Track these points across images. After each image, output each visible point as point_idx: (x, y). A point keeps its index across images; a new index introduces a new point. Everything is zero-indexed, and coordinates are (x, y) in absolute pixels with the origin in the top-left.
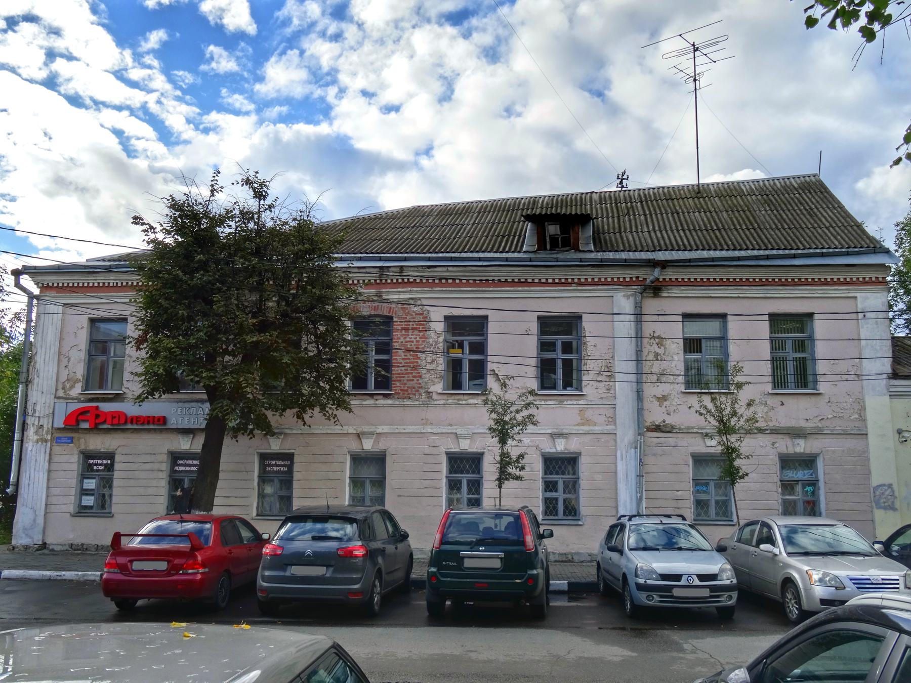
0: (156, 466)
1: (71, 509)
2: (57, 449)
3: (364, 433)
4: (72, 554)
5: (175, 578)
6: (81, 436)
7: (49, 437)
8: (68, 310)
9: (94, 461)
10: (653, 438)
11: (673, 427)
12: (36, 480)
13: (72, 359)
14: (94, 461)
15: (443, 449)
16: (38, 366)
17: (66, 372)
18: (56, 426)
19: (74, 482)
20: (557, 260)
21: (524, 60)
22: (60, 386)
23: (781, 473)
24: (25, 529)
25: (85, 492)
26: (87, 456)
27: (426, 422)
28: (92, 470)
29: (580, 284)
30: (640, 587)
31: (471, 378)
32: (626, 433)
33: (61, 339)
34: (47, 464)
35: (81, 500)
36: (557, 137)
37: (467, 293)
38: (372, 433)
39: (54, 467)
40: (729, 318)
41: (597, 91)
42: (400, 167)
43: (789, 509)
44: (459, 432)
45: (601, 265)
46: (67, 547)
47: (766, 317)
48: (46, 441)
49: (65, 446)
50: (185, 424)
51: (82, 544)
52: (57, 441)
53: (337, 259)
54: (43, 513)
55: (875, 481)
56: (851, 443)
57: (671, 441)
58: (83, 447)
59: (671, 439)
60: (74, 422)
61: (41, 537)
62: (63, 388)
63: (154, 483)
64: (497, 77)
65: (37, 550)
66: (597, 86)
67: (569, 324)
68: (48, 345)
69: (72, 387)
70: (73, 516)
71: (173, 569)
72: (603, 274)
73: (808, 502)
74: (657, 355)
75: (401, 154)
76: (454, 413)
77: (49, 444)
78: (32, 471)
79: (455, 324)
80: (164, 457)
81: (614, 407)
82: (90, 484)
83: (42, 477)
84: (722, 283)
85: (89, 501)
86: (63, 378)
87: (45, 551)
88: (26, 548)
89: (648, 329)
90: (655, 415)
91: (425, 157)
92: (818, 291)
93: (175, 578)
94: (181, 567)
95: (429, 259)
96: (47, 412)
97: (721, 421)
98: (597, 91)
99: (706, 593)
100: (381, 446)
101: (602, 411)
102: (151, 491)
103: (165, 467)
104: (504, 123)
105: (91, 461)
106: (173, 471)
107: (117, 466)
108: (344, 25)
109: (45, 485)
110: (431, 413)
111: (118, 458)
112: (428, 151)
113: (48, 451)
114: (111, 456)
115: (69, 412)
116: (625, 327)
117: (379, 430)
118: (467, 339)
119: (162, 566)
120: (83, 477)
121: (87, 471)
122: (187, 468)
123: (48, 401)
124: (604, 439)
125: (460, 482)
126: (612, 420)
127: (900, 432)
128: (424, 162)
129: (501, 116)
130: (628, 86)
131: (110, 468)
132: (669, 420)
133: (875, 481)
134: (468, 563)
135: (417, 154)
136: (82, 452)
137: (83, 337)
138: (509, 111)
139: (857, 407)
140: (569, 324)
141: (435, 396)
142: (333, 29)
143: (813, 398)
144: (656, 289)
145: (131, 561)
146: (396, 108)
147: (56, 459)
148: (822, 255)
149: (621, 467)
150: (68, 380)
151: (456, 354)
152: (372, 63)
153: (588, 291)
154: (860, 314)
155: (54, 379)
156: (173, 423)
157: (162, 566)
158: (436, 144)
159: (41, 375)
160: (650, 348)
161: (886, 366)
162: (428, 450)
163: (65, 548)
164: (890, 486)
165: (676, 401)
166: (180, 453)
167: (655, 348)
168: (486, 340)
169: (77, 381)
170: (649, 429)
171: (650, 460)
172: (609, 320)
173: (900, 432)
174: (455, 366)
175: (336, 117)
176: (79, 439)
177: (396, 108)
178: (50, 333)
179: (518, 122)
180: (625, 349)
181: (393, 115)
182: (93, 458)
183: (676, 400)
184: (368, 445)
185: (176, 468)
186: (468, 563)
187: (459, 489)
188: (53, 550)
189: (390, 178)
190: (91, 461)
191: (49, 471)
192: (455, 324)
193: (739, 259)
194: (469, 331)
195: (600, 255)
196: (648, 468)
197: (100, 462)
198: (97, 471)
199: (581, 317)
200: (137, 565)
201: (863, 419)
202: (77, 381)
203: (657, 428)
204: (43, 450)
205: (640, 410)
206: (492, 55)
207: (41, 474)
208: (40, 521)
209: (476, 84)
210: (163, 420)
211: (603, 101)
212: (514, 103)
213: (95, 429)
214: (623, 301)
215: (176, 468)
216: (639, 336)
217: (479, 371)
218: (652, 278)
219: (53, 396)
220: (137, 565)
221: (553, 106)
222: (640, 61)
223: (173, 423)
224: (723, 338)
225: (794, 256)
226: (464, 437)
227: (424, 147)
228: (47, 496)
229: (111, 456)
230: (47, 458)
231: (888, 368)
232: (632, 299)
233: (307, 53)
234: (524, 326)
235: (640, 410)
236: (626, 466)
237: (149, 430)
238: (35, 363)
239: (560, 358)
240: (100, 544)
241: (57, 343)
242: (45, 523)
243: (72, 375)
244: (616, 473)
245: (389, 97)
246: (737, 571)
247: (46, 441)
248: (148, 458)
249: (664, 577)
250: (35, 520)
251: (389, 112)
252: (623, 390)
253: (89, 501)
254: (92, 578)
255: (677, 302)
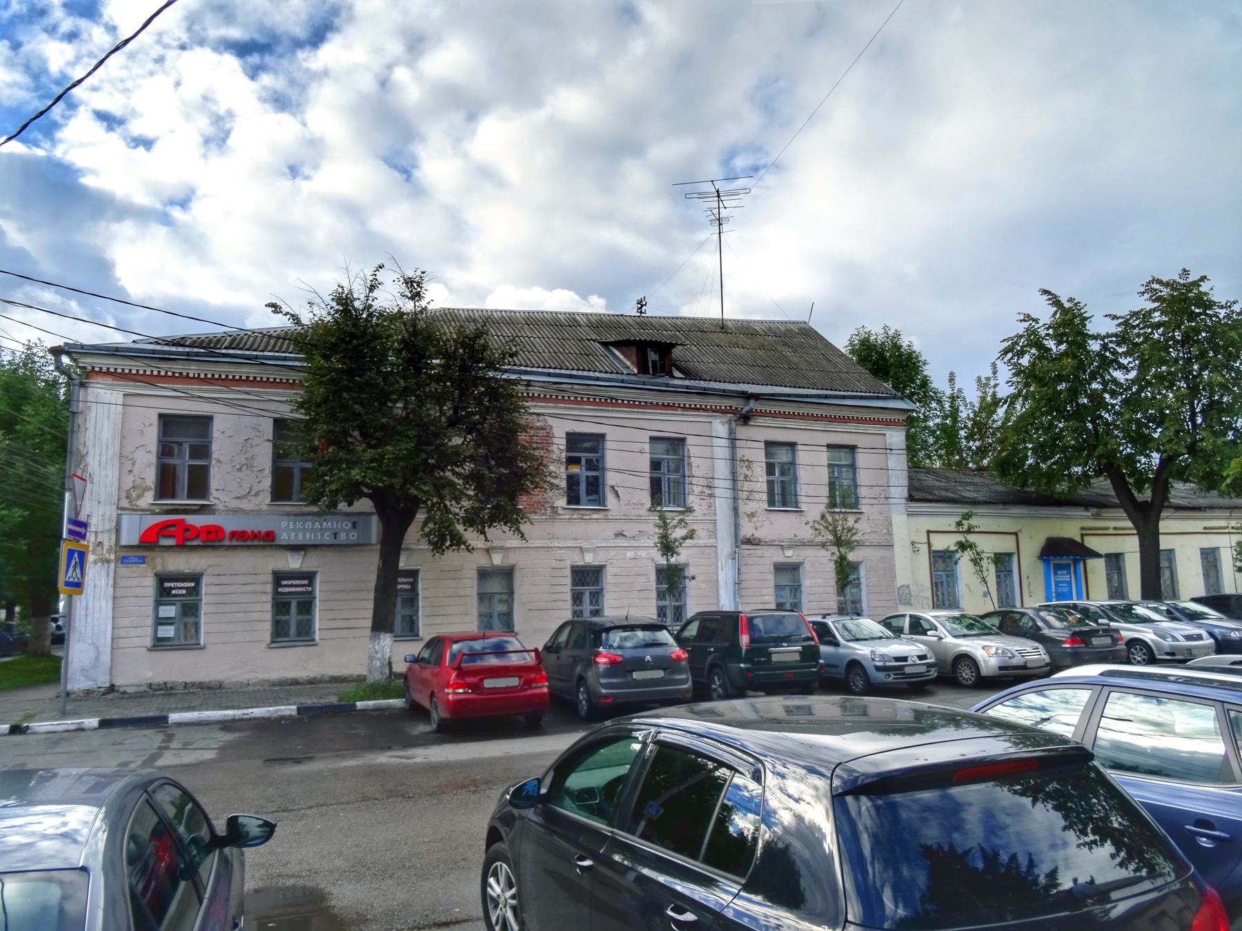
0: (259, 588)
1: (148, 642)
2: (123, 571)
3: (494, 548)
4: (153, 696)
5: (529, 692)
6: (157, 554)
7: (112, 557)
8: (130, 401)
9: (172, 585)
10: (746, 550)
11: (760, 540)
12: (97, 609)
13: (138, 462)
14: (172, 585)
15: (569, 563)
16: (90, 469)
17: (131, 478)
18: (124, 542)
19: (150, 610)
20: (667, 385)
21: (326, 115)
22: (124, 495)
23: (479, 586)
24: (83, 670)
25: (167, 621)
26: (162, 579)
27: (553, 537)
28: (169, 595)
29: (684, 408)
30: (878, 669)
31: (588, 493)
32: (725, 546)
33: (123, 438)
34: (111, 590)
35: (156, 631)
36: (350, 210)
37: (588, 411)
38: (502, 548)
39: (120, 593)
40: (800, 447)
41: (402, 166)
42: (142, 215)
43: (842, 611)
44: (584, 545)
45: (688, 392)
46: (144, 688)
47: (762, 445)
48: (108, 561)
49: (135, 568)
50: (300, 539)
51: (165, 683)
52: (123, 561)
53: (506, 371)
54: (108, 649)
55: (899, 583)
56: (881, 553)
57: (759, 553)
58: (159, 568)
59: (759, 551)
60: (150, 540)
61: (107, 678)
62: (127, 497)
63: (258, 607)
64: (284, 128)
65: (104, 694)
66: (403, 162)
67: (677, 443)
68: (104, 441)
69: (140, 496)
70: (150, 650)
71: (528, 683)
72: (703, 398)
73: (485, 615)
74: (746, 476)
75: (142, 199)
76: (578, 528)
77: (113, 565)
78: (91, 599)
79: (574, 440)
80: (270, 578)
81: (714, 522)
82: (169, 611)
83: (105, 606)
84: (774, 415)
85: (168, 631)
86: (128, 484)
87: (115, 695)
88: (88, 693)
89: (740, 453)
90: (747, 530)
91: (178, 208)
92: (862, 428)
93: (529, 692)
94: (534, 680)
95: (549, 375)
96: (107, 527)
97: (835, 536)
98: (402, 166)
99: (924, 669)
100: (512, 560)
101: (705, 526)
102: (253, 616)
103: (269, 588)
104: (287, 184)
105: (167, 585)
106: (276, 593)
107: (204, 589)
108: (83, 23)
109: (110, 614)
110: (559, 528)
111: (205, 580)
112: (184, 204)
113: (112, 574)
114: (196, 578)
115: (145, 528)
116: (721, 449)
117: (508, 545)
118: (584, 456)
119: (514, 682)
120: (158, 604)
121: (163, 594)
122: (293, 589)
123: (108, 513)
124: (707, 551)
125: (289, 603)
126: (713, 534)
127: (913, 543)
128: (176, 213)
129: (283, 174)
130: (438, 167)
131: (195, 591)
132: (758, 534)
133: (899, 583)
134: (775, 658)
135: (172, 203)
136: (157, 575)
137: (152, 436)
138: (294, 171)
139: (886, 523)
140: (677, 443)
141: (560, 511)
142: (67, 25)
143: (795, 515)
144: (745, 419)
145: (482, 680)
146: (147, 143)
147: (122, 582)
148: (862, 398)
149: (721, 576)
150: (133, 487)
151: (575, 470)
152: (122, 81)
153: (692, 417)
154: (888, 449)
155: (116, 486)
156: (284, 538)
157: (514, 682)
158: (199, 193)
159: (96, 480)
160: (742, 471)
161: (904, 492)
162: (555, 564)
163: (142, 689)
164: (908, 586)
165: (761, 518)
166: (284, 572)
167: (744, 470)
168: (603, 457)
169: (147, 489)
170: (743, 543)
171: (743, 569)
172: (709, 443)
173: (913, 543)
174: (572, 481)
175: (60, 141)
176: (154, 559)
177: (147, 143)
178: (106, 427)
179: (305, 186)
180: (722, 469)
181: (141, 149)
182: (170, 580)
183: (762, 516)
184: (497, 560)
185: (280, 590)
186: (775, 658)
187: (288, 612)
188: (124, 693)
189: (127, 228)
190: (167, 585)
191: (114, 598)
192: (574, 440)
193: (807, 396)
194: (586, 448)
195: (687, 383)
196: (743, 577)
197: (179, 585)
198: (175, 595)
199: (683, 440)
200: (489, 683)
201: (890, 533)
202: (147, 489)
203: (748, 542)
204: (104, 573)
205: (737, 527)
206: (280, 102)
207: (104, 603)
208: (106, 658)
209: (262, 131)
210: (270, 536)
211: (407, 180)
212: (303, 163)
213: (181, 547)
214: (720, 427)
215: (280, 590)
216: (733, 459)
217: (595, 488)
218: (747, 408)
219: (114, 507)
220: (489, 683)
221: (350, 173)
222: (457, 141)
223: (284, 538)
224: (853, 467)
225: (844, 397)
226: (589, 550)
227: (180, 195)
228: (113, 628)
229: (196, 578)
230: (111, 582)
231: (905, 494)
232: (727, 426)
233: (26, 48)
234: (637, 447)
235: (737, 527)
236: (725, 575)
237: (249, 547)
238: (86, 465)
239: (667, 479)
240: (188, 681)
241: (117, 442)
242: (112, 660)
243: (139, 481)
244: (717, 581)
245: (136, 128)
246: (935, 654)
247: (108, 561)
248: (249, 579)
249: (897, 659)
250: (97, 658)
251: (135, 147)
252: (722, 506)
253: (168, 631)
254: (288, 713)
255: (762, 431)
